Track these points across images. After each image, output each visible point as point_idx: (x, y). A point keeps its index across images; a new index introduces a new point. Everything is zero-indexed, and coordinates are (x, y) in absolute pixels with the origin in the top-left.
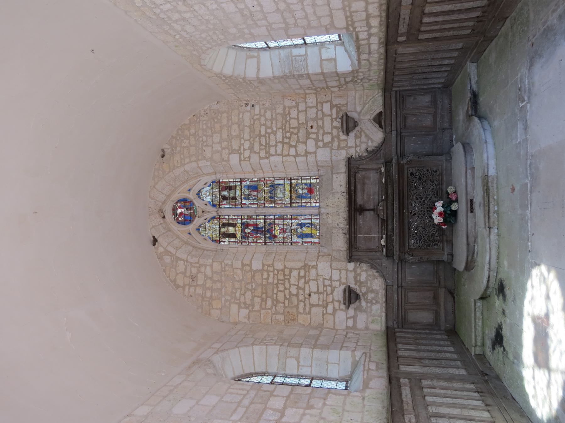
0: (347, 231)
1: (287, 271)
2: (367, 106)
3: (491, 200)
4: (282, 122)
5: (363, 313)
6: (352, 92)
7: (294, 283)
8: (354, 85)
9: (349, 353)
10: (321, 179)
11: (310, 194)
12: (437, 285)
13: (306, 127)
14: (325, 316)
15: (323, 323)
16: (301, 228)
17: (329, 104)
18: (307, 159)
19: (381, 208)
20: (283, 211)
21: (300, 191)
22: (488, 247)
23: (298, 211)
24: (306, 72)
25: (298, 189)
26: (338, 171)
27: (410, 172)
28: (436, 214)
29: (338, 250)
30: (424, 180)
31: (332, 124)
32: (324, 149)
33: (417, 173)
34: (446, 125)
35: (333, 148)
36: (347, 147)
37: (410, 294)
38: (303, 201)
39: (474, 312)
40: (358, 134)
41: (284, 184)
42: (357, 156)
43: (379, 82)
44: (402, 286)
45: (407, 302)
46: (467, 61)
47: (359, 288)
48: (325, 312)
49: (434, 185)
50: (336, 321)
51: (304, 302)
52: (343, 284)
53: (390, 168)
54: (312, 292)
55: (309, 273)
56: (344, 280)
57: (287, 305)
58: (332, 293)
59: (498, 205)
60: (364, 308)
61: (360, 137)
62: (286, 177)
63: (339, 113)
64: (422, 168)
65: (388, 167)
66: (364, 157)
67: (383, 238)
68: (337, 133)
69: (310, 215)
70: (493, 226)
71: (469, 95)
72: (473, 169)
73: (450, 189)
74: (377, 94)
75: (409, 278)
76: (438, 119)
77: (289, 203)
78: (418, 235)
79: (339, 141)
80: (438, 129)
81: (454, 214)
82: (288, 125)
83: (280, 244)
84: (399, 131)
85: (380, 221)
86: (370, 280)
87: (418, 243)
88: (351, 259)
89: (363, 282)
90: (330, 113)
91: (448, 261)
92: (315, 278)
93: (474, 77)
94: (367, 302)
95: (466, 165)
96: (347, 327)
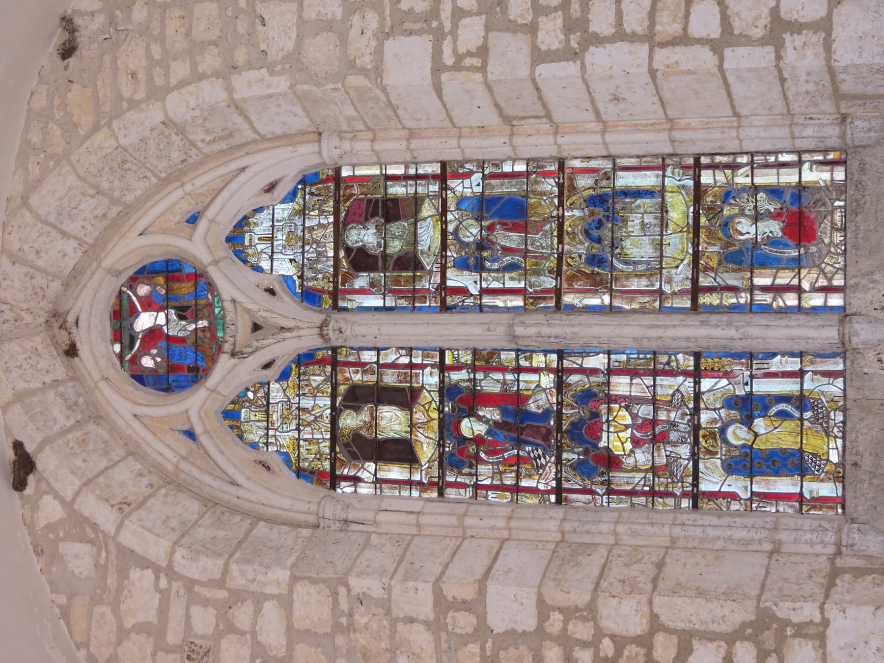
10: (854, 164)
11: (798, 246)
16: (748, 421)
18: (779, 58)
21: (746, 229)
23: (732, 333)
25: (732, 218)
38: (759, 281)
41: (663, 190)
62: (671, 155)
69: (792, 355)
77: (682, 292)
83: (636, 500)
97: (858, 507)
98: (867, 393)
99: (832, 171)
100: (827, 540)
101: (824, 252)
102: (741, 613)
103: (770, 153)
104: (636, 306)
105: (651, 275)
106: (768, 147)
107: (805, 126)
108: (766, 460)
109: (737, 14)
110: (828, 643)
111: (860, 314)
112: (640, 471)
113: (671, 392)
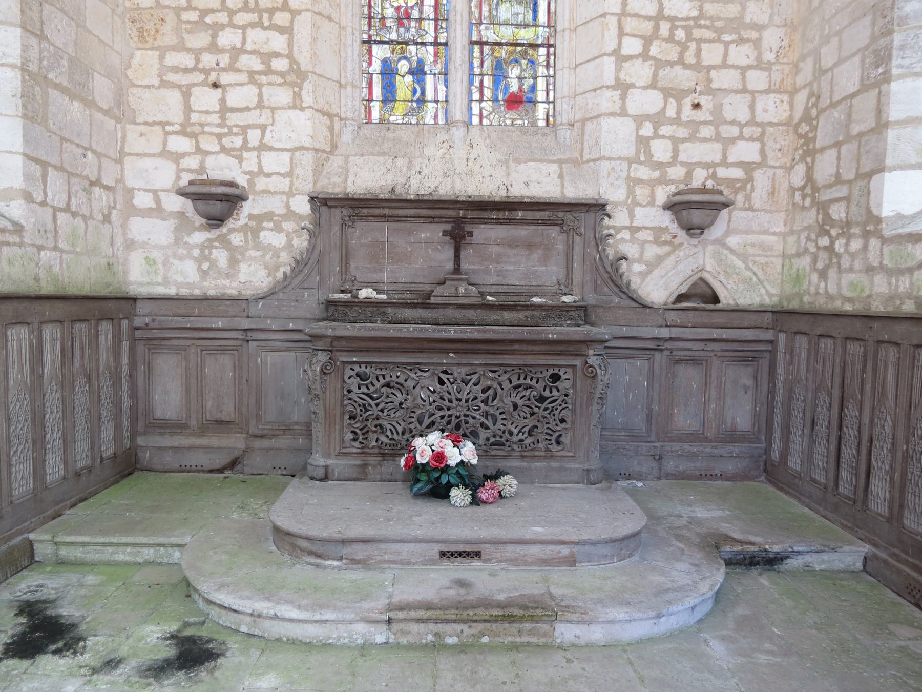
0: (401, 194)
1: (282, 18)
2: (739, 263)
3: (480, 627)
4: (719, 19)
5: (172, 236)
6: (782, 224)
7: (249, 40)
8: (808, 228)
9: (18, 182)
10: (547, 130)
11: (505, 101)
12: (252, 430)
13: (698, 89)
14: (157, 128)
15: (139, 124)
16: (411, 72)
17: (756, 158)
18: (608, 87)
19: (462, 290)
20: (459, 20)
21: (514, 72)
22: (329, 616)
23: (458, 62)
24: (895, 72)
25: (521, 64)
26: (566, 178)
27: (561, 373)
28: (441, 445)
29: (347, 171)
30: (536, 410)
31: (699, 164)
32: (633, 138)
33: (558, 391)
34: (670, 465)
35: (634, 165)
36: (632, 205)
37: (226, 361)
38: (486, 79)
39: (151, 542)
40: (667, 237)
41: (536, 26)
42: (606, 232)
43: (806, 299)
44: (248, 341)
45: (204, 352)
46: (875, 545)
47: (242, 227)
48: (168, 128)
49: (521, 436)
50: (147, 159)
51: (195, 69)
52: (251, 182)
53: (570, 319)
54: (224, 91)
55: (279, 85)
56: (261, 183)
57: (185, 16)
58: (224, 150)
59: (461, 649)
60: (186, 239)
61: (657, 242)
62: (555, 30)
63: (728, 186)
64: (570, 407)
65: (573, 313)
66: (604, 250)
67: (378, 293)
68: (673, 177)
69: (447, 97)
70: (394, 630)
71: (776, 548)
72: (571, 561)
73: (508, 483)
74: (767, 291)
75: (270, 358)
76: (686, 446)
77: (480, 36)
78: (384, 390)
79: (652, 184)
80: (661, 444)
81: (440, 493)
82: (708, 34)
83: (366, 9)
84: (668, 345)
85: (427, 288)
86: (263, 256)
87: (359, 388)
88: (320, 202)
89: (258, 237)
90: (731, 160)
91: (309, 466)
92: (266, 103)
93: (823, 562)
94: (202, 247)
95: (584, 543)
96: (130, 192)
97: (367, 130)
98: (427, 135)
99: (544, 119)
100: (348, 113)
101: (501, 115)
102: (305, 63)
103: (554, 86)
104: (473, 9)
105: (490, 18)
106: (558, 84)
107: (568, 104)
108: (390, 82)
109: (633, 65)
110: (291, 111)
111: (468, 132)
112: (382, 11)
113: (426, 29)
